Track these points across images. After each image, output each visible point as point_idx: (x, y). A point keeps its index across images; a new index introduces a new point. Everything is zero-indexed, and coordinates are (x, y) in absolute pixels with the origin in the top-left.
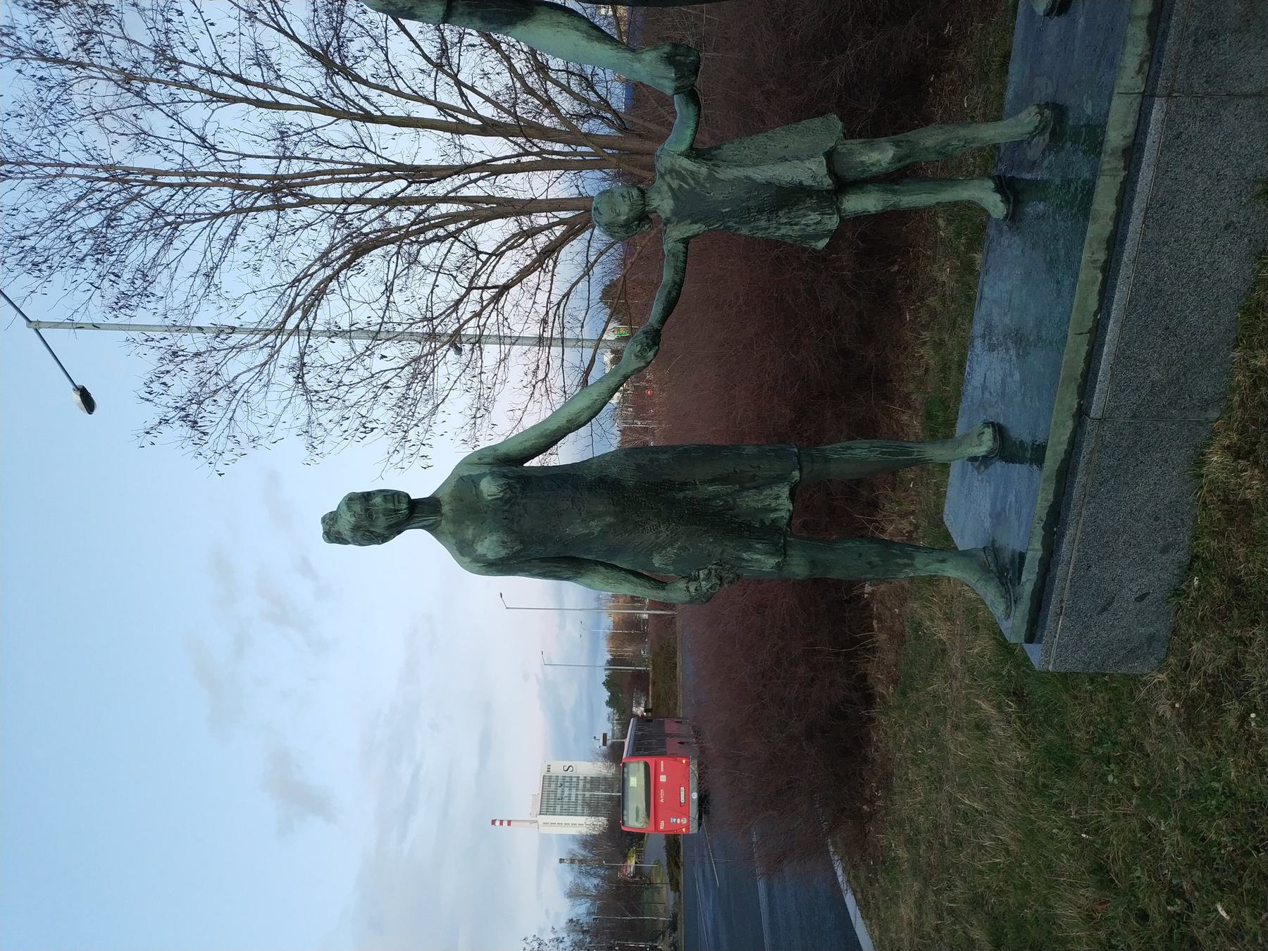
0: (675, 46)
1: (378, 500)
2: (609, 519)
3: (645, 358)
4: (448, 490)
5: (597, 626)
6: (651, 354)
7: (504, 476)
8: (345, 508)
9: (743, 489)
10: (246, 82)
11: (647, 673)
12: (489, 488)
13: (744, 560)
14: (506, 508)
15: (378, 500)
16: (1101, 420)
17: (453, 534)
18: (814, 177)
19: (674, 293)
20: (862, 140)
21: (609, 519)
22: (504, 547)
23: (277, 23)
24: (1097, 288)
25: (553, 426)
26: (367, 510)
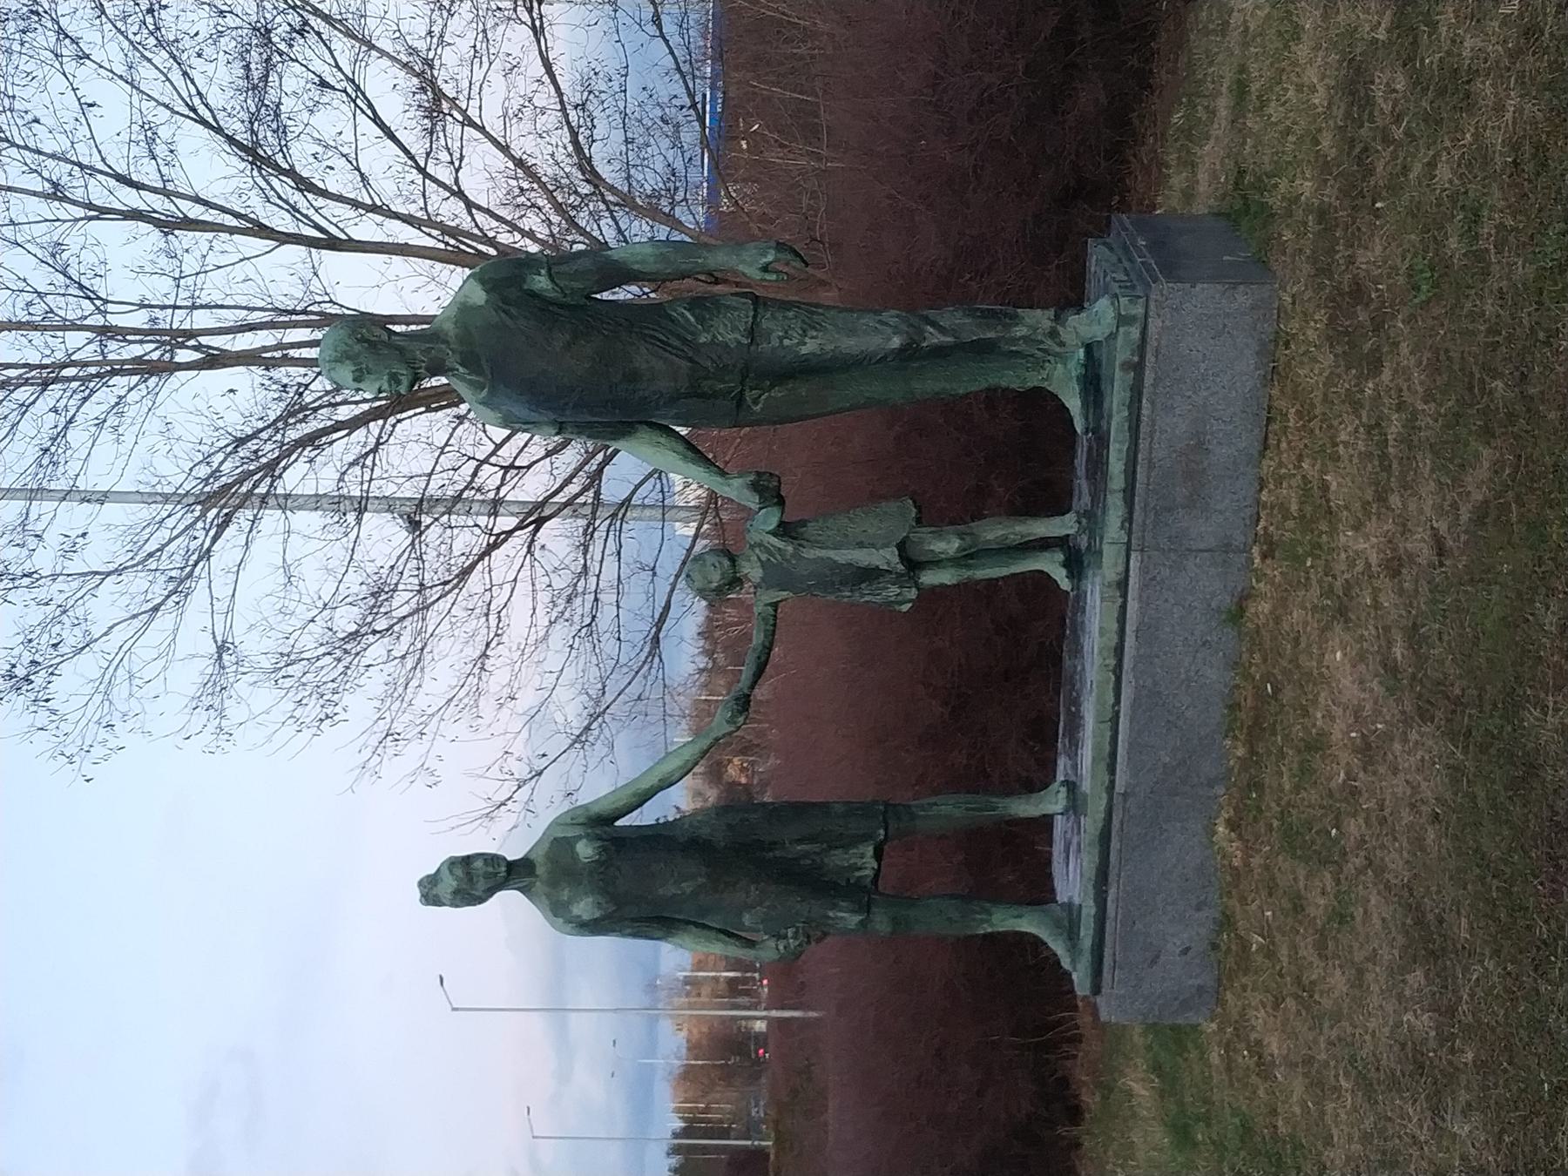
0: (758, 474)
1: (479, 864)
2: (701, 880)
3: (735, 723)
4: (541, 852)
5: (651, 1048)
6: (741, 719)
7: (599, 838)
8: (445, 872)
9: (830, 848)
10: (138, 186)
11: (761, 1154)
12: (585, 851)
13: (829, 917)
14: (602, 869)
15: (479, 864)
16: (1125, 795)
17: (548, 896)
18: (888, 563)
19: (763, 659)
20: (933, 529)
21: (701, 880)
22: (599, 908)
23: (194, 110)
24: (1111, 685)
25: (645, 785)
26: (468, 874)
